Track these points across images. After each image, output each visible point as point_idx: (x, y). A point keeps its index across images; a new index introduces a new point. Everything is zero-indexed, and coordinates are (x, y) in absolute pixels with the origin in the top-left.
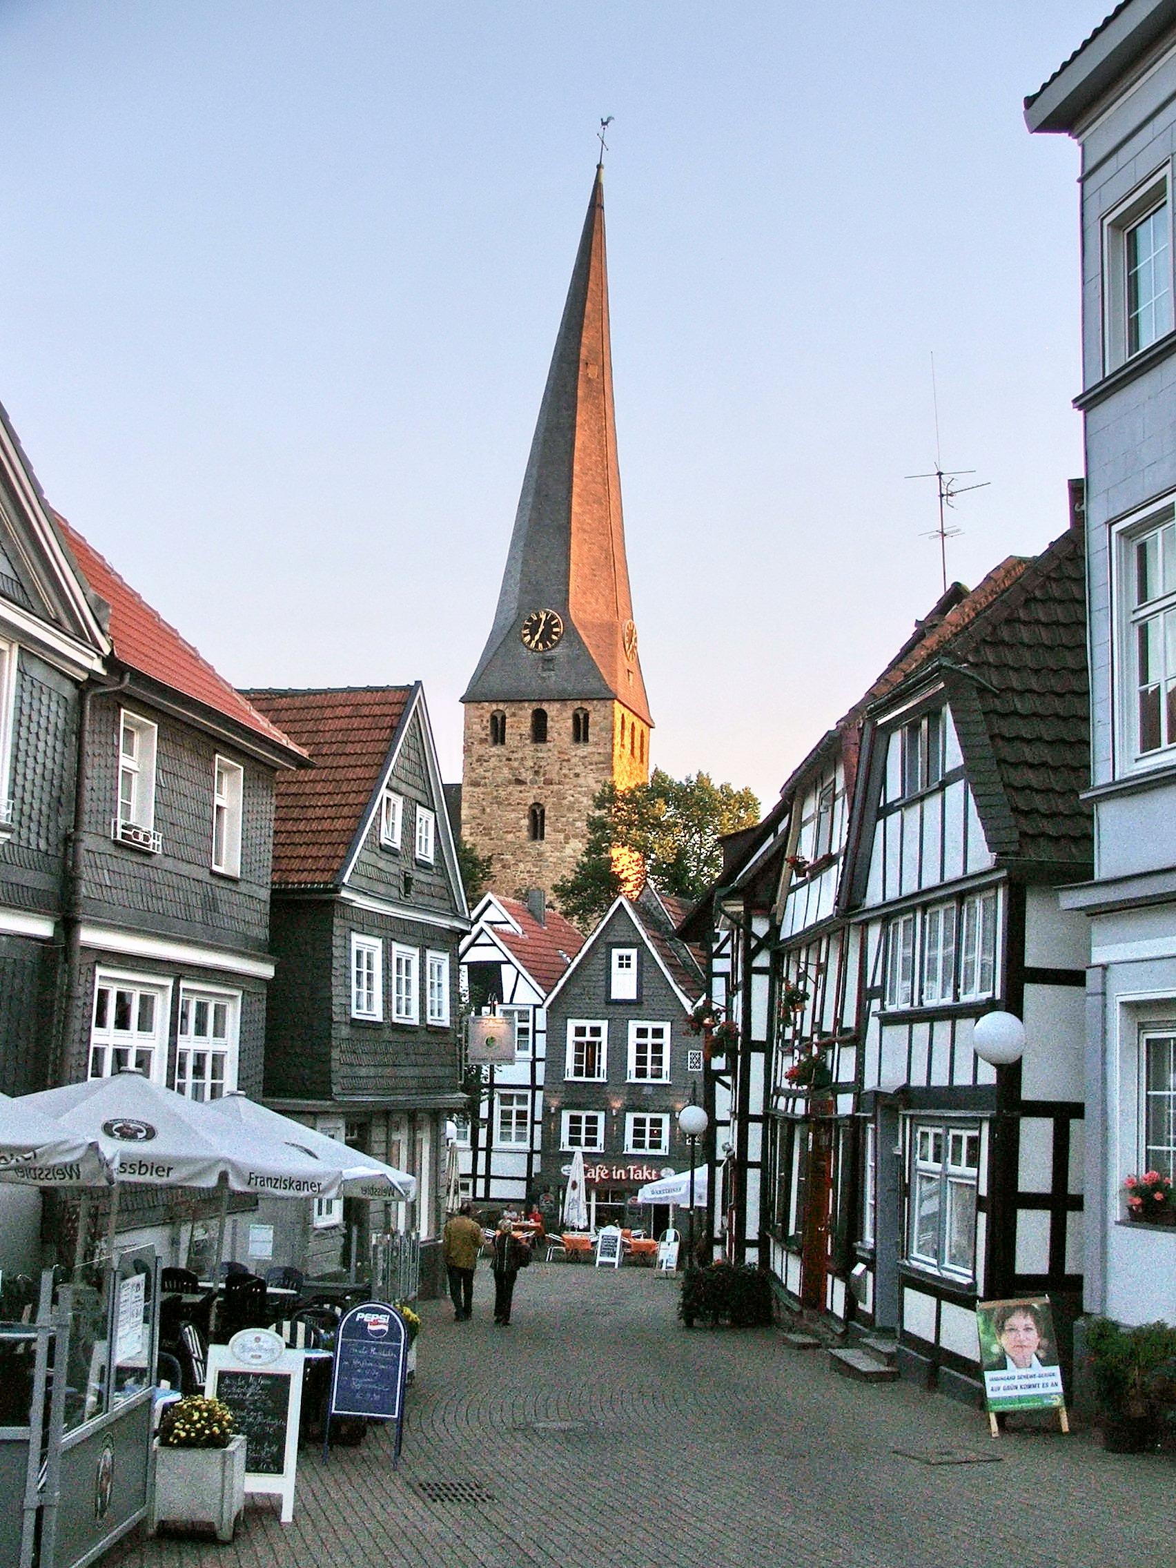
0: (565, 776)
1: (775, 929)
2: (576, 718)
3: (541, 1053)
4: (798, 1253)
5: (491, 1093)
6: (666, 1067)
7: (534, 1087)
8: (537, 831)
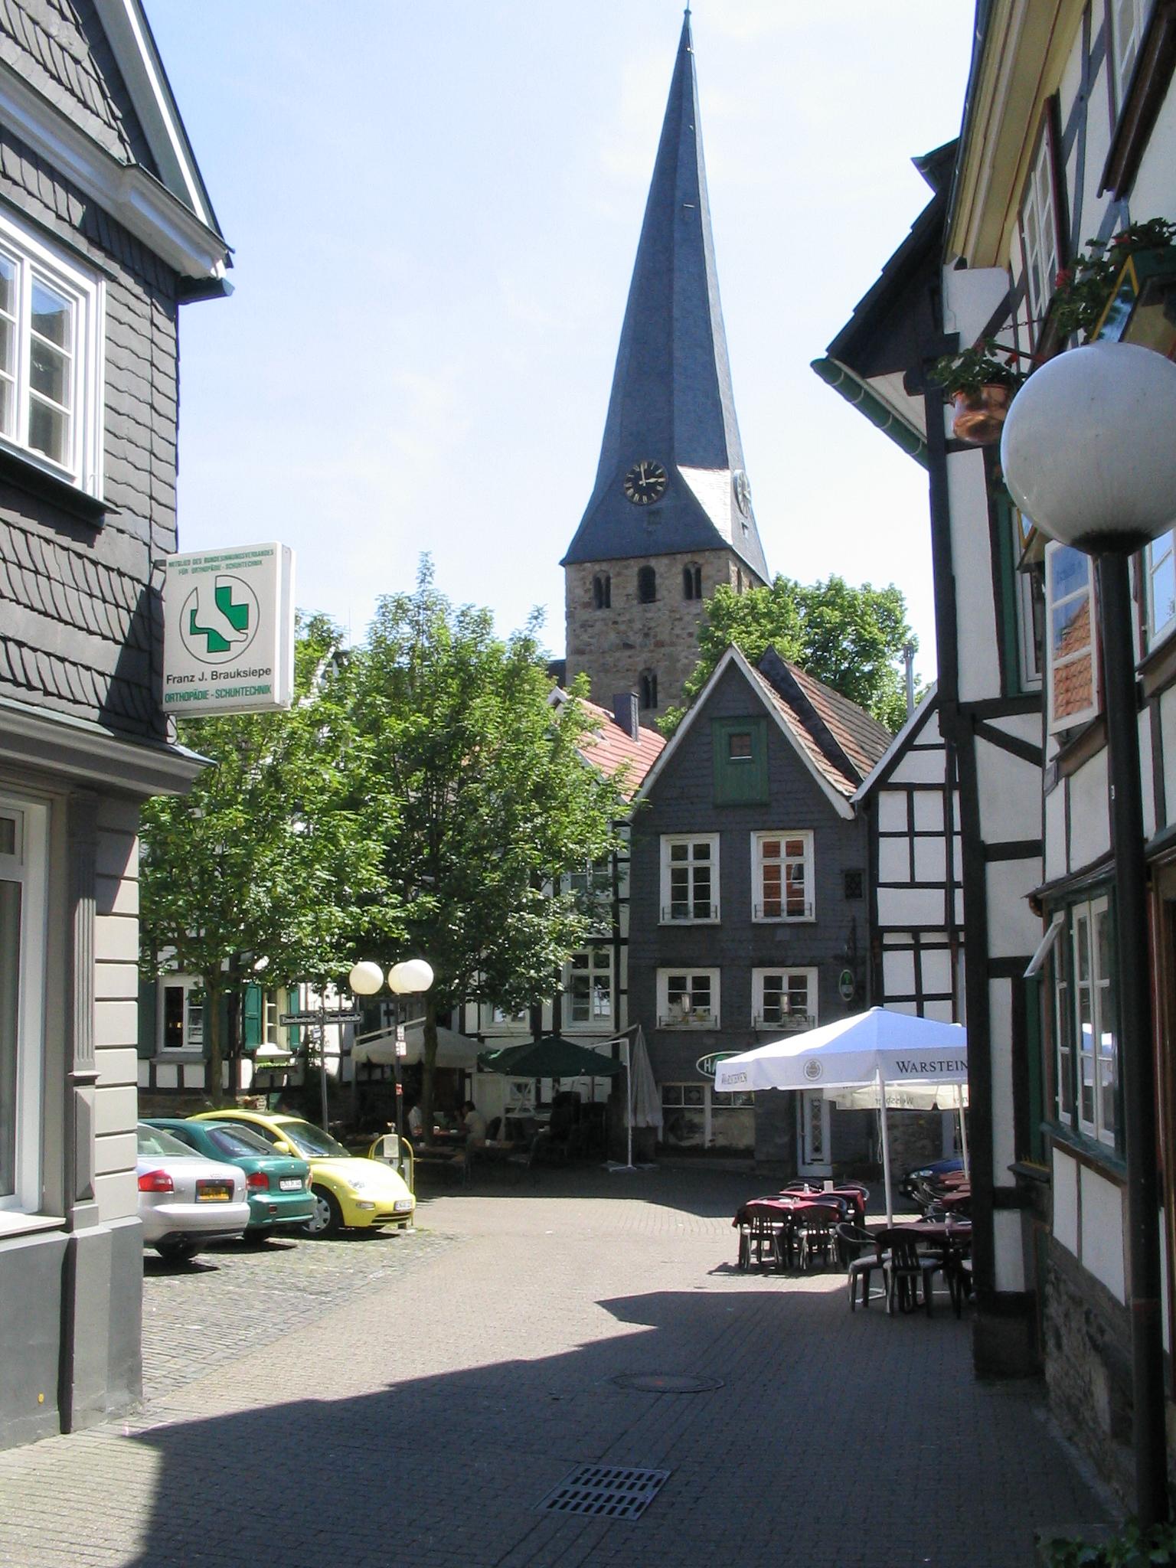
0: (678, 636)
2: (687, 574)
6: (810, 897)
7: (617, 941)
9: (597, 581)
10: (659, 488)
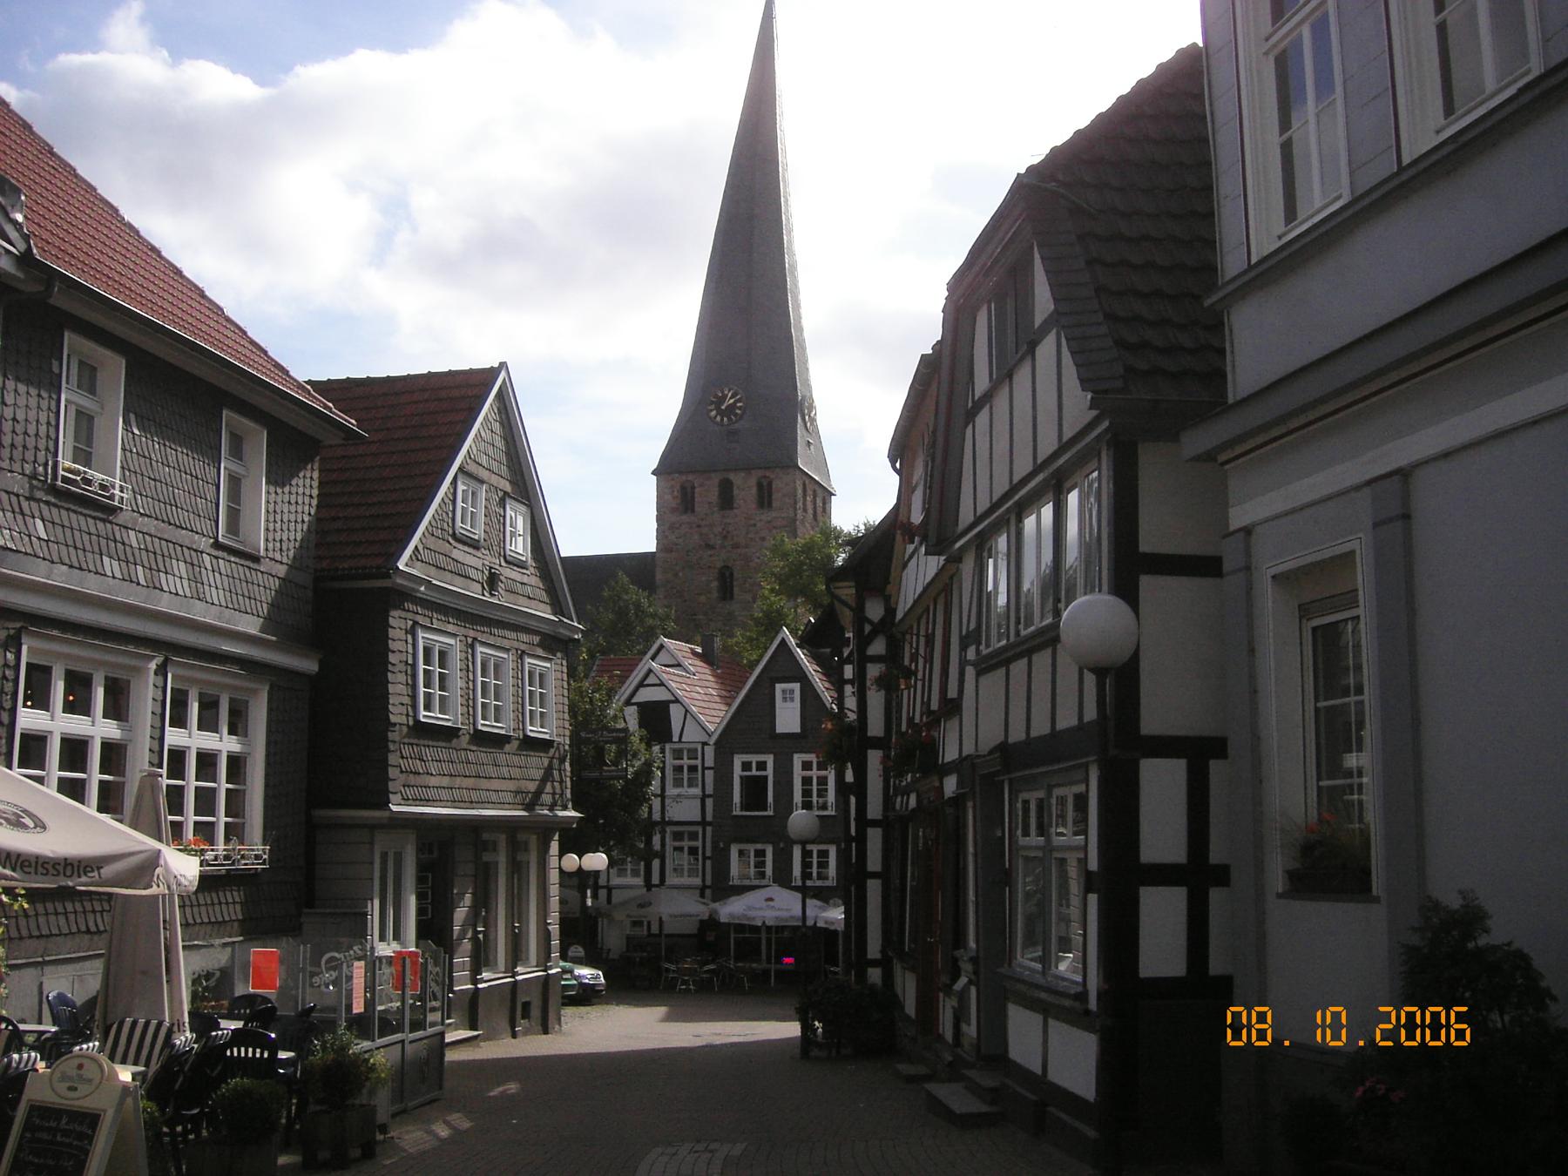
0: (751, 539)
1: (890, 611)
2: (760, 485)
3: (709, 790)
4: (913, 969)
5: (663, 833)
7: (703, 823)
8: (726, 592)
9: (683, 488)
10: (739, 405)
